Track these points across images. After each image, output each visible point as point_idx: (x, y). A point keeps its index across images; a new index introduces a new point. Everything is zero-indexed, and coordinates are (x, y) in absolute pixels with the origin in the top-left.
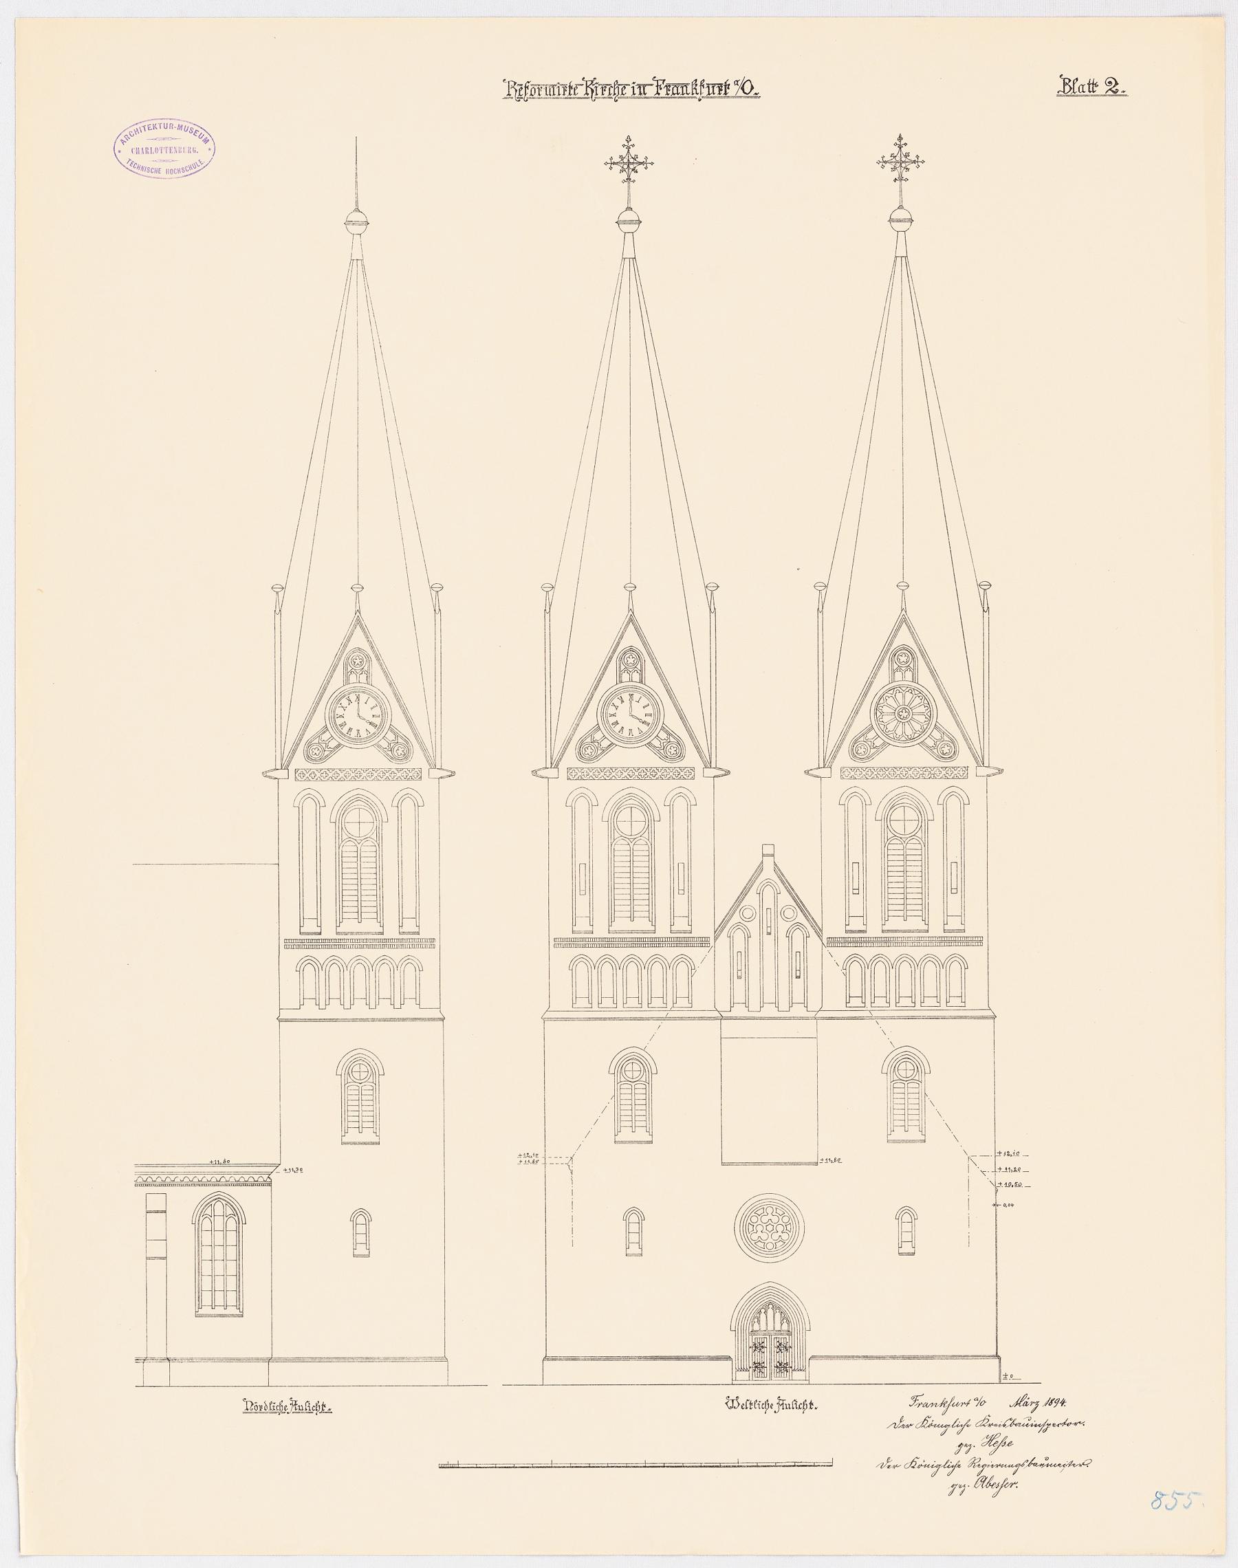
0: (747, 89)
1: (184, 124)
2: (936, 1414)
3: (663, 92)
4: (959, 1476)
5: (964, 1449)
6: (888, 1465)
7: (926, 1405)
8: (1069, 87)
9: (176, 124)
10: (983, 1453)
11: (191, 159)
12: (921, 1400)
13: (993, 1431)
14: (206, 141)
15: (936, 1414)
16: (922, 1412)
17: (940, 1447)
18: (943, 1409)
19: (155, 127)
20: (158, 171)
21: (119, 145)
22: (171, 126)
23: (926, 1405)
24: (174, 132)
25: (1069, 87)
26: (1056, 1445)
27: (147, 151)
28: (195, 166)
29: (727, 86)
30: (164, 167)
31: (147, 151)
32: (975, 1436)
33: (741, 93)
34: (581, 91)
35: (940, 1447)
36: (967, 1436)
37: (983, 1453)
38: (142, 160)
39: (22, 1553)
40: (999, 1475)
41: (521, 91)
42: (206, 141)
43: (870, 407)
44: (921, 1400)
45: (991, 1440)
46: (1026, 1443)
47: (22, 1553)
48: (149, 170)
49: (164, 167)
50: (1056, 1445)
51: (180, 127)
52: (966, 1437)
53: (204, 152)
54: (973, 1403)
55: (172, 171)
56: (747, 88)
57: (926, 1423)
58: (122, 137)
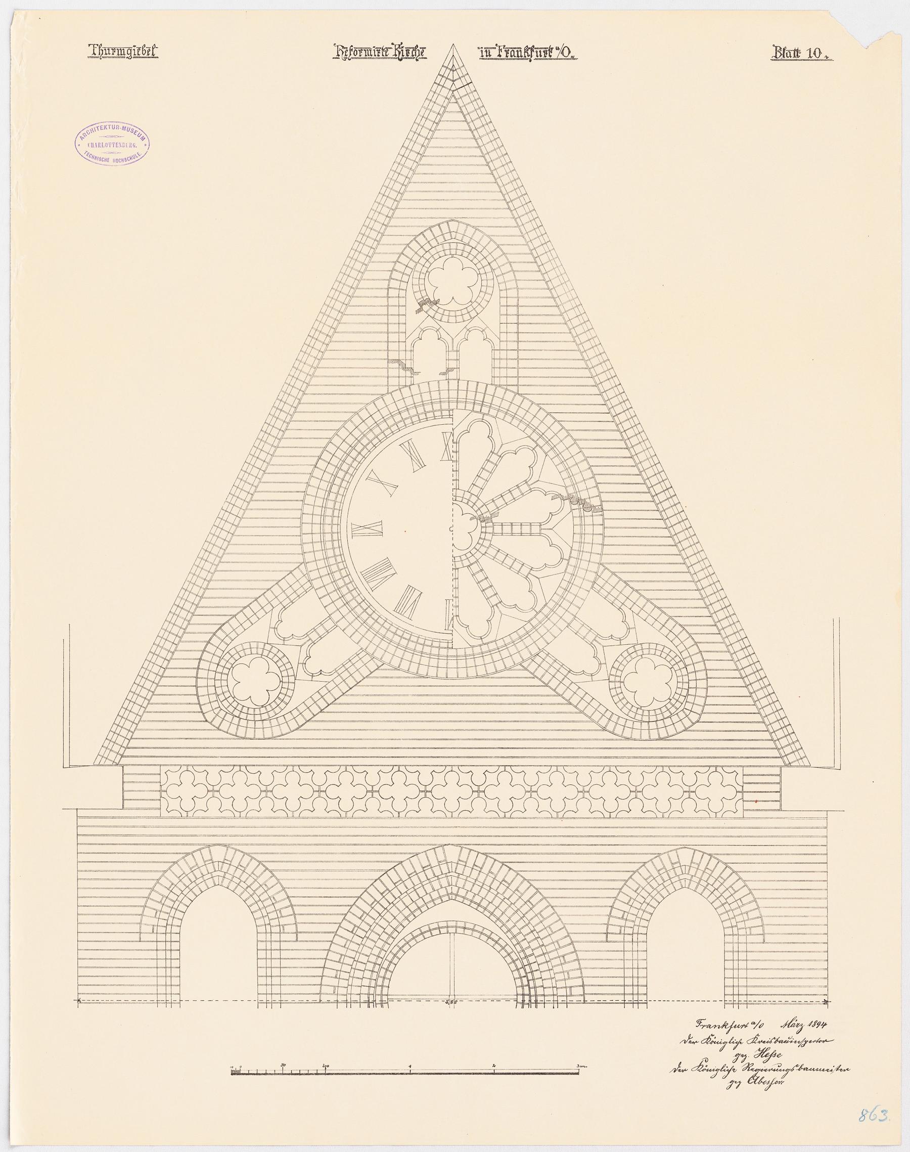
0: (566, 54)
1: (127, 126)
2: (721, 1035)
3: (503, 54)
4: (732, 1076)
5: (734, 1085)
6: (678, 1069)
7: (709, 1026)
8: (781, 54)
9: (121, 126)
10: (758, 1063)
11: (133, 152)
12: (703, 1023)
13: (762, 1046)
14: (143, 139)
15: (721, 1035)
16: (707, 1032)
17: (720, 1058)
18: (725, 1030)
19: (105, 127)
20: (107, 160)
21: (79, 141)
22: (118, 127)
23: (709, 1026)
24: (120, 132)
25: (781, 54)
26: (811, 1056)
27: (99, 145)
28: (134, 156)
29: (551, 49)
30: (112, 157)
31: (99, 145)
32: (751, 1050)
33: (561, 56)
34: (391, 53)
35: (720, 1058)
36: (740, 1049)
37: (758, 1063)
38: (96, 152)
39: (13, 1142)
40: (768, 1076)
41: (149, 53)
42: (143, 139)
43: (837, 744)
44: (703, 1023)
45: (762, 1053)
46: (790, 1055)
47: (13, 1142)
48: (101, 159)
49: (112, 157)
50: (811, 1056)
51: (124, 128)
52: (740, 1049)
53: (141, 148)
54: (751, 1026)
55: (117, 160)
56: (566, 52)
57: (709, 1040)
58: (81, 135)
